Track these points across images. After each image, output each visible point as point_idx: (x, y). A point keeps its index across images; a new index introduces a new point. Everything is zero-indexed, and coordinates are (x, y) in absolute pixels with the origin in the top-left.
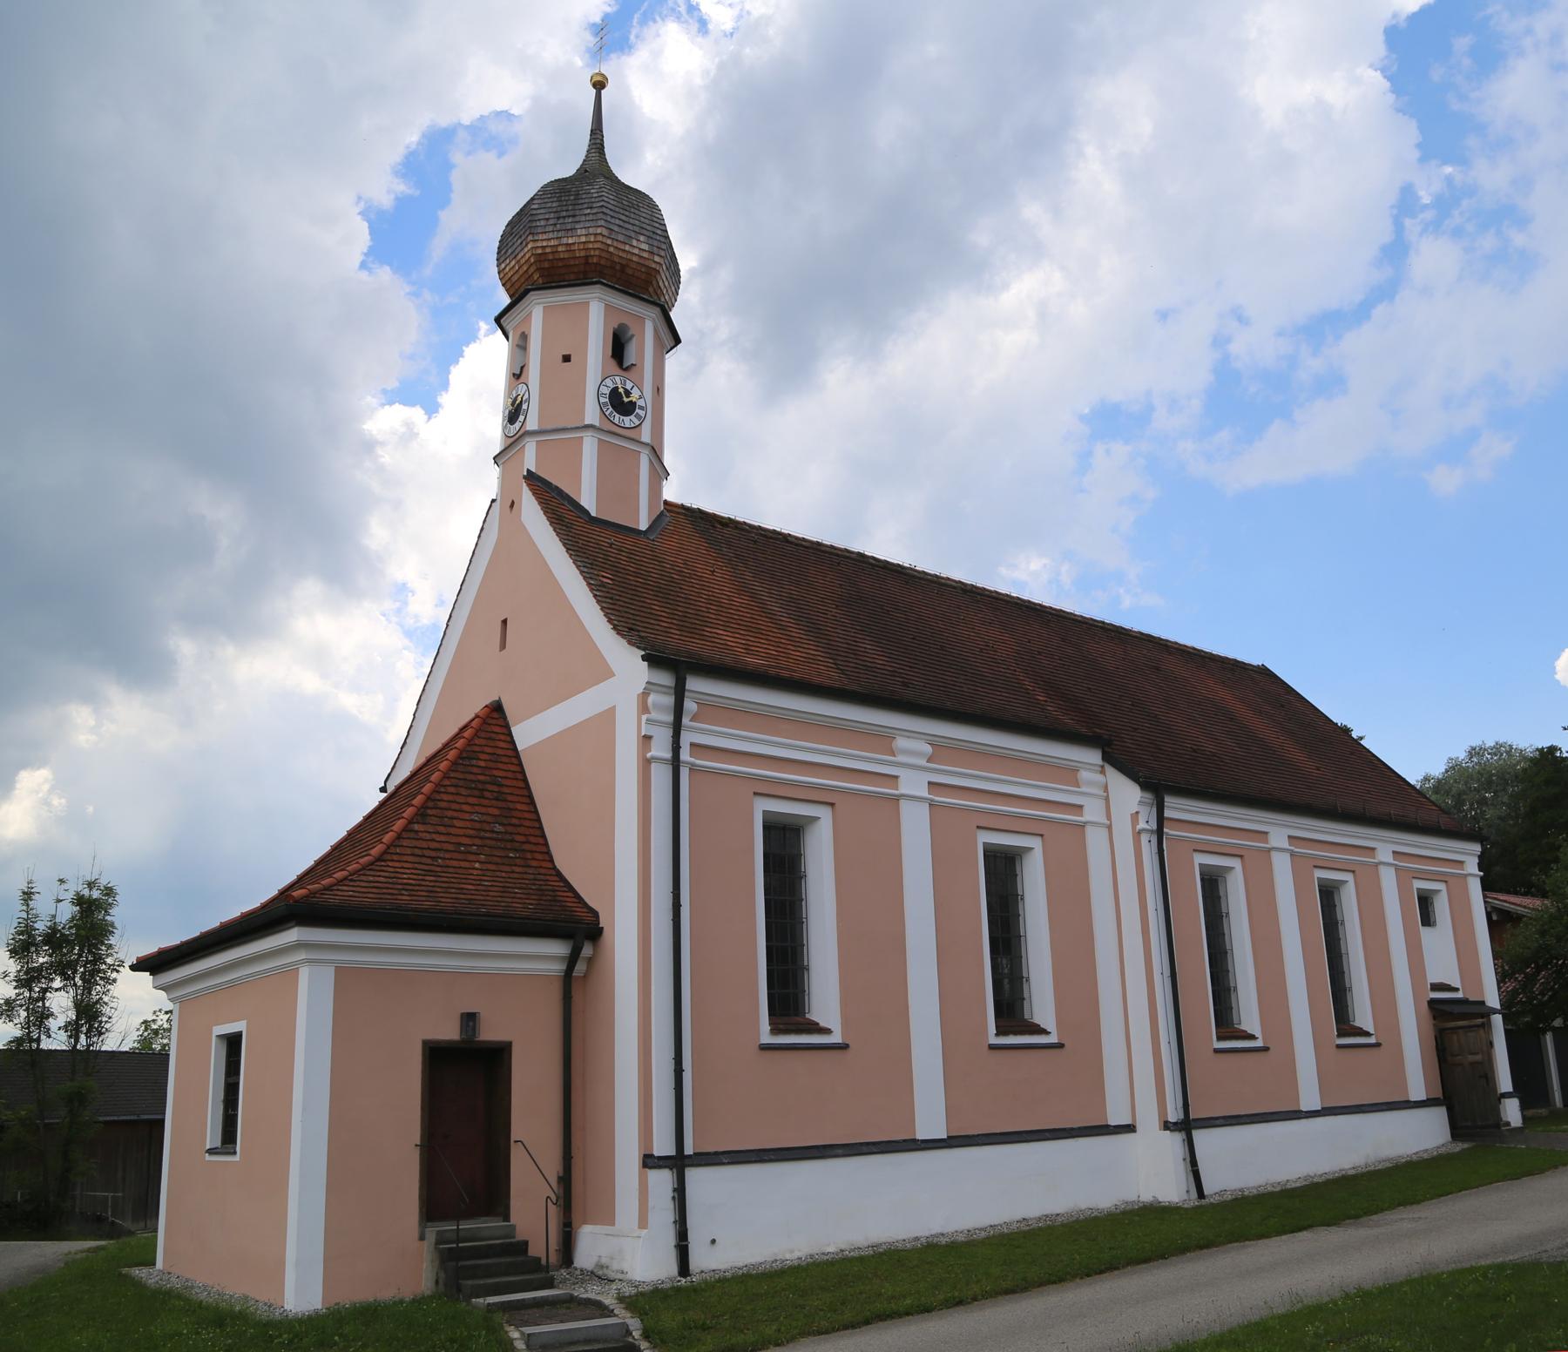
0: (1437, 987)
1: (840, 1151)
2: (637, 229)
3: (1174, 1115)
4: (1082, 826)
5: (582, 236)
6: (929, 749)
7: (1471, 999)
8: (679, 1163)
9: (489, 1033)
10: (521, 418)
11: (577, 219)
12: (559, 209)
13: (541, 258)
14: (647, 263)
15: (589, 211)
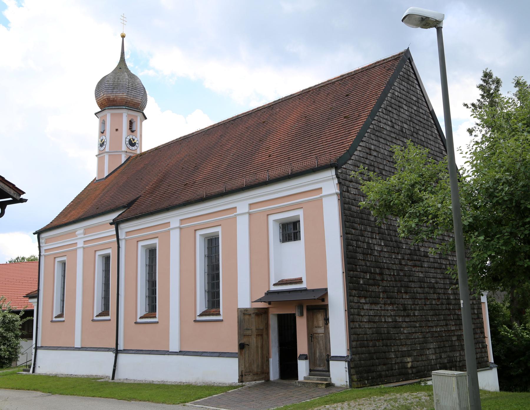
5: (121, 95)
10: (104, 146)
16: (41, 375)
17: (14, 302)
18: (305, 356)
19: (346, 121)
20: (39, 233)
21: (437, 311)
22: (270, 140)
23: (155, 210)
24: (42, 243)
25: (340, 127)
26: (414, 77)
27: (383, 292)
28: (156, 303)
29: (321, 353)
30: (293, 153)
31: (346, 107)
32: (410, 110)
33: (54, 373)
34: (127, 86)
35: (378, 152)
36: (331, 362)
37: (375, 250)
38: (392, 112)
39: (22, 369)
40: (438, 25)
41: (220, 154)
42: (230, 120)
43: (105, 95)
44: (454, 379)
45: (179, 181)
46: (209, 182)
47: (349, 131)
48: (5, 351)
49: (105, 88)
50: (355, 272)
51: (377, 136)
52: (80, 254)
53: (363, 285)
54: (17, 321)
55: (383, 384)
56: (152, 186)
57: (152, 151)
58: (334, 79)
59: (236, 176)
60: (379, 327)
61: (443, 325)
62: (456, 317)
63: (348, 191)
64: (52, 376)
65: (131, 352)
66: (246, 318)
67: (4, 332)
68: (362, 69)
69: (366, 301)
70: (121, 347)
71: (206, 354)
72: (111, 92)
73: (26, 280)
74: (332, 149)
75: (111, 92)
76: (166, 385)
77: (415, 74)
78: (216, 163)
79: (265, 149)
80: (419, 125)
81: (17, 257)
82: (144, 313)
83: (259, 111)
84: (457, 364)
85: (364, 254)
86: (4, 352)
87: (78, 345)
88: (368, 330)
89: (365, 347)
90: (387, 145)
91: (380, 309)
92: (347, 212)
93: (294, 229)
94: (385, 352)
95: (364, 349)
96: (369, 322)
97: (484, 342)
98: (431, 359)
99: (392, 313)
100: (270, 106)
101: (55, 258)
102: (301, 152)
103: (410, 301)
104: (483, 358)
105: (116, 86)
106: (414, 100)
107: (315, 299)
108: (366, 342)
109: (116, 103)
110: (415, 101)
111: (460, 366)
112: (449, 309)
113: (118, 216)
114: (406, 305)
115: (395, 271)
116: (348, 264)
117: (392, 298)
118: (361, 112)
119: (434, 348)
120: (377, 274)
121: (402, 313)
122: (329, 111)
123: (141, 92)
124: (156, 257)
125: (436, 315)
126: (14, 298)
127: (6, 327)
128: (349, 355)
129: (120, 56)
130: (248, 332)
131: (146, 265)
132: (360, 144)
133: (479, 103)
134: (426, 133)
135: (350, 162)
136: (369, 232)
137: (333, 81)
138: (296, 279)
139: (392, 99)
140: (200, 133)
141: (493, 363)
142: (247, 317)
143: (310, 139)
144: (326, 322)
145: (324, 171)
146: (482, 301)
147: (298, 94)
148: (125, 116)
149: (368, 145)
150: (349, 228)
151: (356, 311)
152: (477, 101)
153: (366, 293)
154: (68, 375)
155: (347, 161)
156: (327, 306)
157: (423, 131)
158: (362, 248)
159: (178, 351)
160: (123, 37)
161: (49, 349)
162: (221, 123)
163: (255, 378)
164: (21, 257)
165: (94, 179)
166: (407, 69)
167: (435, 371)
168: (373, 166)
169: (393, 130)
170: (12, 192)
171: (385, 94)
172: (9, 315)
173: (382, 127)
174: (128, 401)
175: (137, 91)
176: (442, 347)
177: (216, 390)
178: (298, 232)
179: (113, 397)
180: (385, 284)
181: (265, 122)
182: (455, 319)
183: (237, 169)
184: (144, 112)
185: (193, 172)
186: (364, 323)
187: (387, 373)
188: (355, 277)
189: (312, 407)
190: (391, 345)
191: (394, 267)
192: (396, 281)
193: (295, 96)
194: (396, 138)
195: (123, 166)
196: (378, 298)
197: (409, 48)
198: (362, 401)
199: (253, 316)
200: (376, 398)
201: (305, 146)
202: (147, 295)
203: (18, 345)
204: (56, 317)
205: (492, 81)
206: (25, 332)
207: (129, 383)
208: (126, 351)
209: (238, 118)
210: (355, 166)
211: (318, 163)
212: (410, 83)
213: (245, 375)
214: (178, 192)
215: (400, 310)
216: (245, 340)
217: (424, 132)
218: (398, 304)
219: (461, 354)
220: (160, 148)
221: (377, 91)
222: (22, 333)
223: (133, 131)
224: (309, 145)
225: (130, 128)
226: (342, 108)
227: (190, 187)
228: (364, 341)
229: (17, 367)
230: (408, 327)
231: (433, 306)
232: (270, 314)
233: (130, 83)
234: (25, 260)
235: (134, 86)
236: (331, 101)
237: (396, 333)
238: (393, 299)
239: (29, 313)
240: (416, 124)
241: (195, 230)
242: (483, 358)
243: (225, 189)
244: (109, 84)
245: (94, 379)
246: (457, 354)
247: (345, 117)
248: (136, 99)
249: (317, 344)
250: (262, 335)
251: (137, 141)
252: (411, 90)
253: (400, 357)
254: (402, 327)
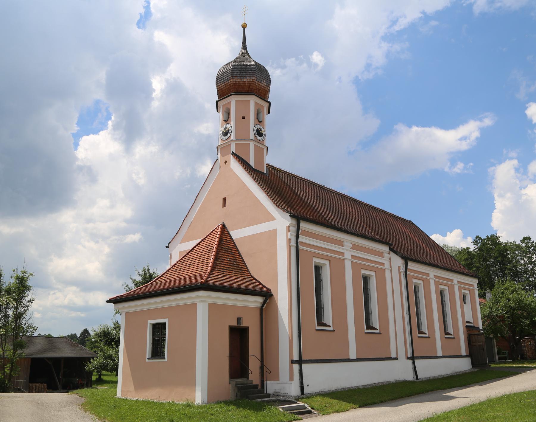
0: (468, 322)
1: (334, 361)
2: (263, 78)
3: (410, 355)
4: (384, 270)
6: (351, 245)
7: (328, 324)
8: (300, 362)
9: (244, 324)
10: (229, 135)
11: (247, 73)
12: (241, 69)
13: (235, 84)
14: (265, 89)
15: (250, 71)
148: (253, 101)
160: (244, 27)
223: (260, 122)
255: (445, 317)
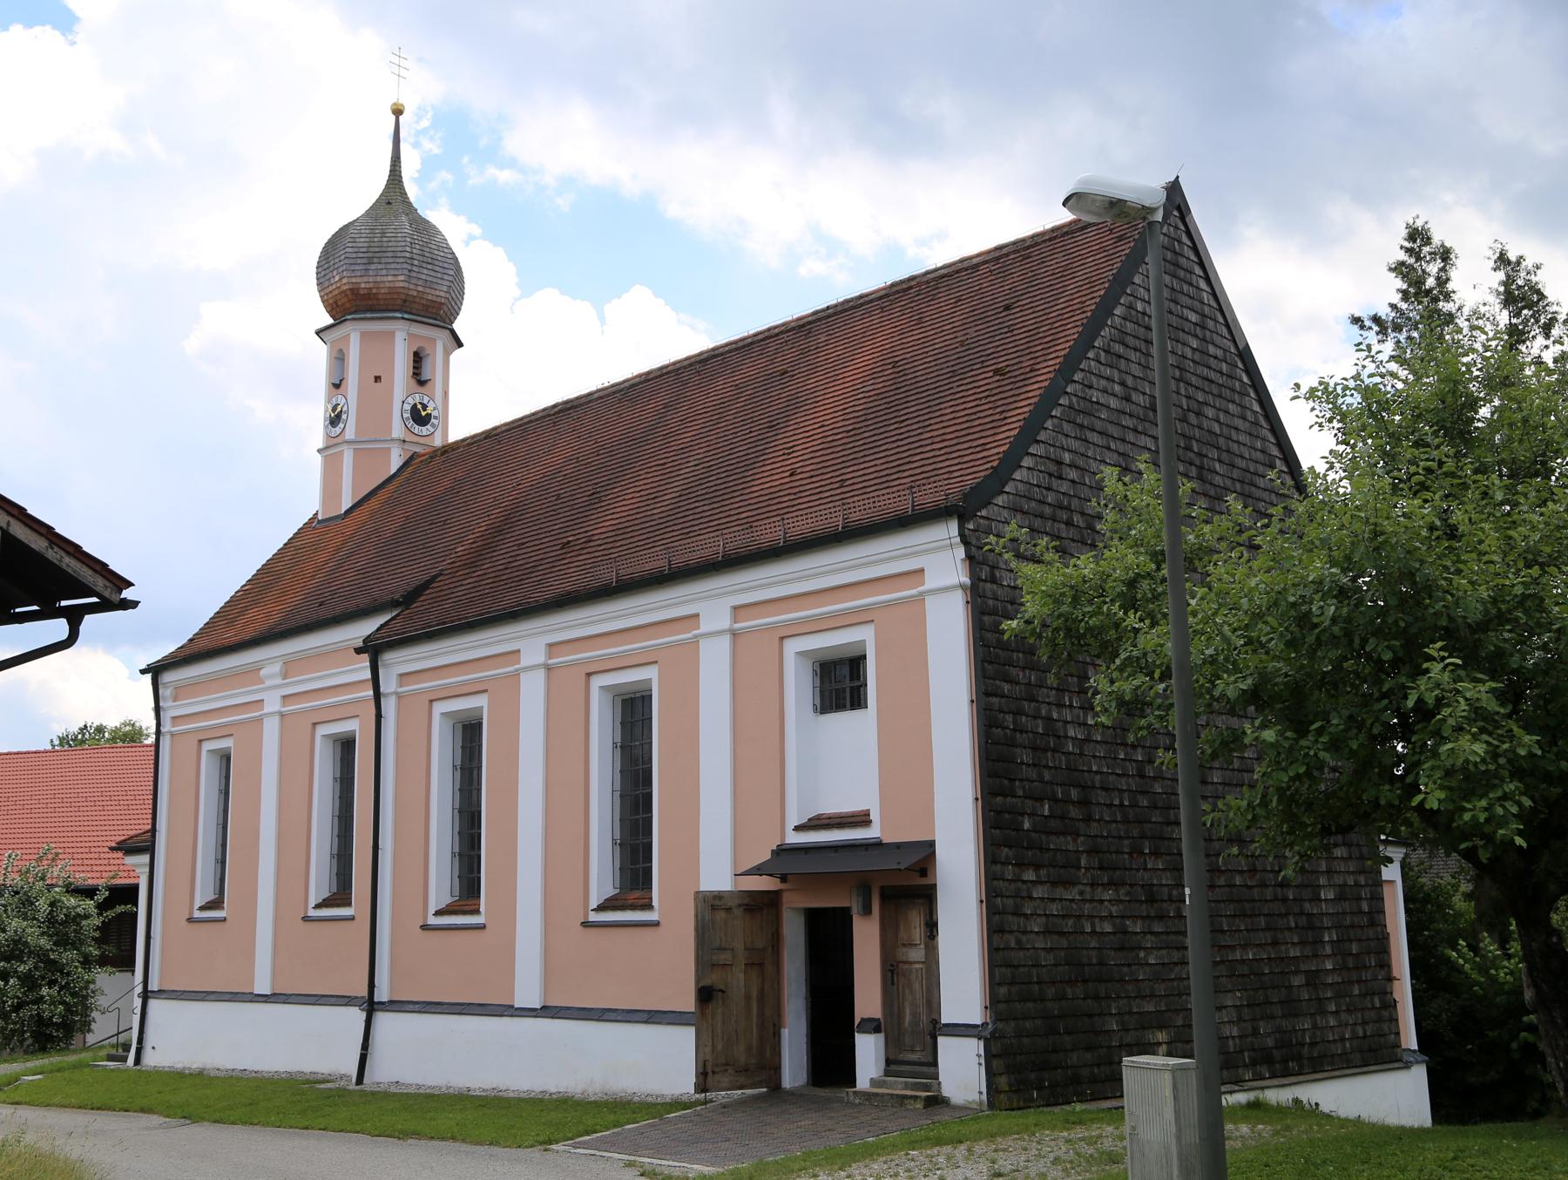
5: (391, 279)
10: (341, 425)
16: (160, 1072)
17: (80, 862)
18: (875, 1024)
19: (998, 384)
20: (155, 671)
21: (1246, 905)
22: (796, 426)
23: (478, 615)
24: (164, 698)
25: (980, 399)
26: (1193, 257)
27: (1089, 852)
28: (479, 872)
29: (914, 1015)
30: (855, 468)
31: (1002, 342)
32: (1179, 349)
33: (194, 1067)
34: (408, 255)
35: (1082, 469)
36: (941, 1040)
37: (1066, 737)
38: (1126, 359)
39: (103, 1053)
40: (1149, 216)
41: (662, 462)
42: (693, 360)
43: (345, 281)
44: (1168, 1076)
45: (548, 534)
46: (628, 541)
47: (1003, 411)
48: (53, 1003)
49: (346, 261)
50: (1009, 799)
51: (1082, 426)
52: (271, 729)
53: (1033, 834)
54: (87, 917)
55: (1080, 1101)
56: (474, 545)
57: (475, 442)
58: (978, 255)
59: (701, 526)
60: (1075, 948)
61: (1265, 944)
62: (1303, 921)
63: (993, 580)
64: (191, 1074)
65: (411, 1007)
66: (718, 918)
67: (51, 949)
68: (1053, 230)
69: (1037, 876)
70: (382, 995)
71: (612, 1016)
72: (363, 273)
73: (113, 798)
74: (956, 461)
75: (363, 273)
76: (504, 1099)
77: (1195, 249)
78: (648, 486)
79: (781, 453)
80: (1207, 389)
81: (82, 725)
82: (446, 900)
83: (771, 337)
84: (1305, 1050)
85: (1035, 749)
86: (50, 1005)
87: (263, 986)
88: (1043, 954)
89: (1034, 1001)
90: (1109, 448)
91: (1078, 897)
92: (989, 635)
93: (852, 679)
94: (1090, 1016)
95: (1030, 1005)
96: (1047, 932)
97: (1386, 993)
98: (1227, 1037)
99: (1114, 909)
100: (803, 326)
101: (200, 741)
102: (876, 465)
103: (1167, 878)
104: (1384, 1035)
105: (378, 255)
106: (1191, 322)
107: (900, 870)
108: (1036, 987)
109: (375, 302)
110: (1196, 324)
111: (1311, 1059)
112: (1285, 900)
113: (378, 629)
114: (1155, 888)
115: (1126, 795)
116: (989, 776)
117: (1115, 869)
118: (1038, 360)
119: (1236, 1006)
120: (1073, 802)
121: (1144, 910)
122: (958, 350)
123: (446, 271)
124: (480, 746)
125: (1245, 915)
126: (80, 850)
127: (57, 934)
128: (988, 1020)
129: (389, 169)
130: (725, 957)
131: (454, 766)
132: (1031, 450)
133: (1393, 314)
134: (1227, 412)
135: (1000, 500)
136: (1052, 689)
137: (975, 261)
138: (853, 815)
139: (1128, 323)
140: (609, 395)
141: (1414, 1051)
142: (721, 915)
143: (902, 430)
144: (932, 932)
145: (928, 524)
146: (1385, 877)
147: (878, 295)
148: (401, 338)
149: (1055, 452)
150: (994, 679)
151: (1010, 902)
152: (1390, 309)
153: (1038, 854)
154: (233, 1070)
155: (993, 497)
156: (932, 888)
157: (1218, 405)
158: (1032, 732)
159: (538, 1006)
160: (398, 112)
161: (182, 997)
162: (667, 366)
163: (742, 1080)
164: (95, 725)
165: (311, 516)
166: (1173, 235)
167: (1129, 1059)
168: (1068, 508)
169: (1128, 408)
170: (99, 583)
171: (1104, 309)
172: (68, 900)
173: (1094, 399)
174: (399, 1138)
175: (437, 269)
176: (1259, 1005)
177: (634, 1113)
178: (861, 686)
179: (358, 1129)
180: (1094, 829)
181: (786, 372)
182: (1300, 925)
183: (705, 508)
184: (456, 326)
185: (588, 508)
186: (1032, 936)
187: (1096, 1071)
188: (1009, 813)
189: (872, 1155)
190: (1108, 997)
191: (1123, 784)
192: (1129, 822)
193: (871, 301)
194: (1135, 430)
195: (395, 483)
196: (1072, 867)
197: (1178, 177)
198: (1008, 1142)
199: (738, 912)
200: (1047, 1136)
201: (887, 450)
202: (457, 850)
203: (92, 986)
204: (202, 908)
205: (1430, 254)
206: (111, 950)
207: (402, 1094)
208: (395, 1006)
209: (715, 356)
210: (1016, 511)
211: (913, 502)
212: (1182, 274)
213: (714, 1073)
214: (544, 567)
215: (1136, 901)
216: (713, 979)
217: (1220, 410)
218: (1131, 885)
219: (1316, 1023)
220: (498, 431)
221: (1084, 299)
222: (103, 953)
223: (422, 383)
224: (898, 446)
225: (414, 373)
226: (990, 346)
227: (577, 553)
228: (1030, 983)
229: (85, 1048)
230: (1161, 948)
231: (1234, 890)
232: (784, 910)
233: (417, 247)
234: (106, 734)
235: (427, 254)
236: (965, 321)
237: (1123, 965)
238: (1118, 872)
239: (128, 894)
240: (1197, 388)
241: (589, 675)
242: (1384, 1035)
243: (670, 565)
244: (356, 250)
245: (308, 1082)
246: (1303, 1025)
247: (996, 372)
248: (433, 292)
249: (907, 991)
250: (761, 965)
251: (435, 409)
252: (1183, 293)
253: (1136, 1029)
254: (1141, 948)
255: (222, 808)
